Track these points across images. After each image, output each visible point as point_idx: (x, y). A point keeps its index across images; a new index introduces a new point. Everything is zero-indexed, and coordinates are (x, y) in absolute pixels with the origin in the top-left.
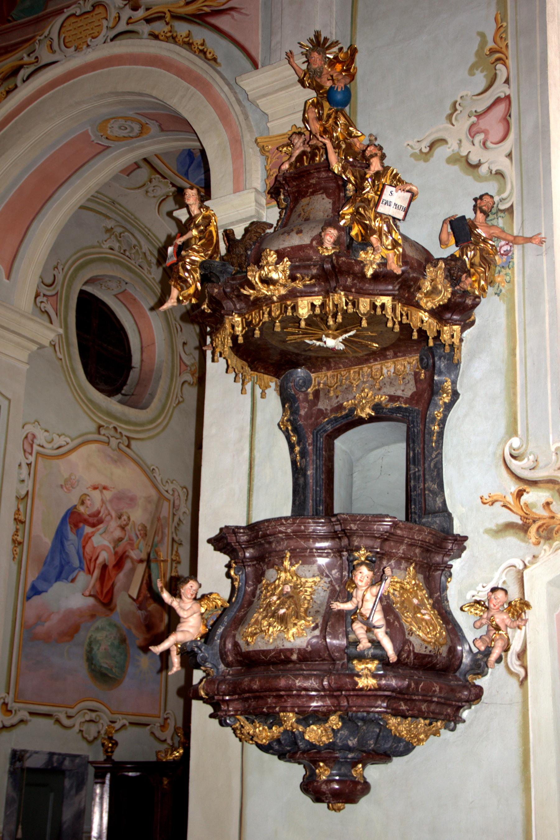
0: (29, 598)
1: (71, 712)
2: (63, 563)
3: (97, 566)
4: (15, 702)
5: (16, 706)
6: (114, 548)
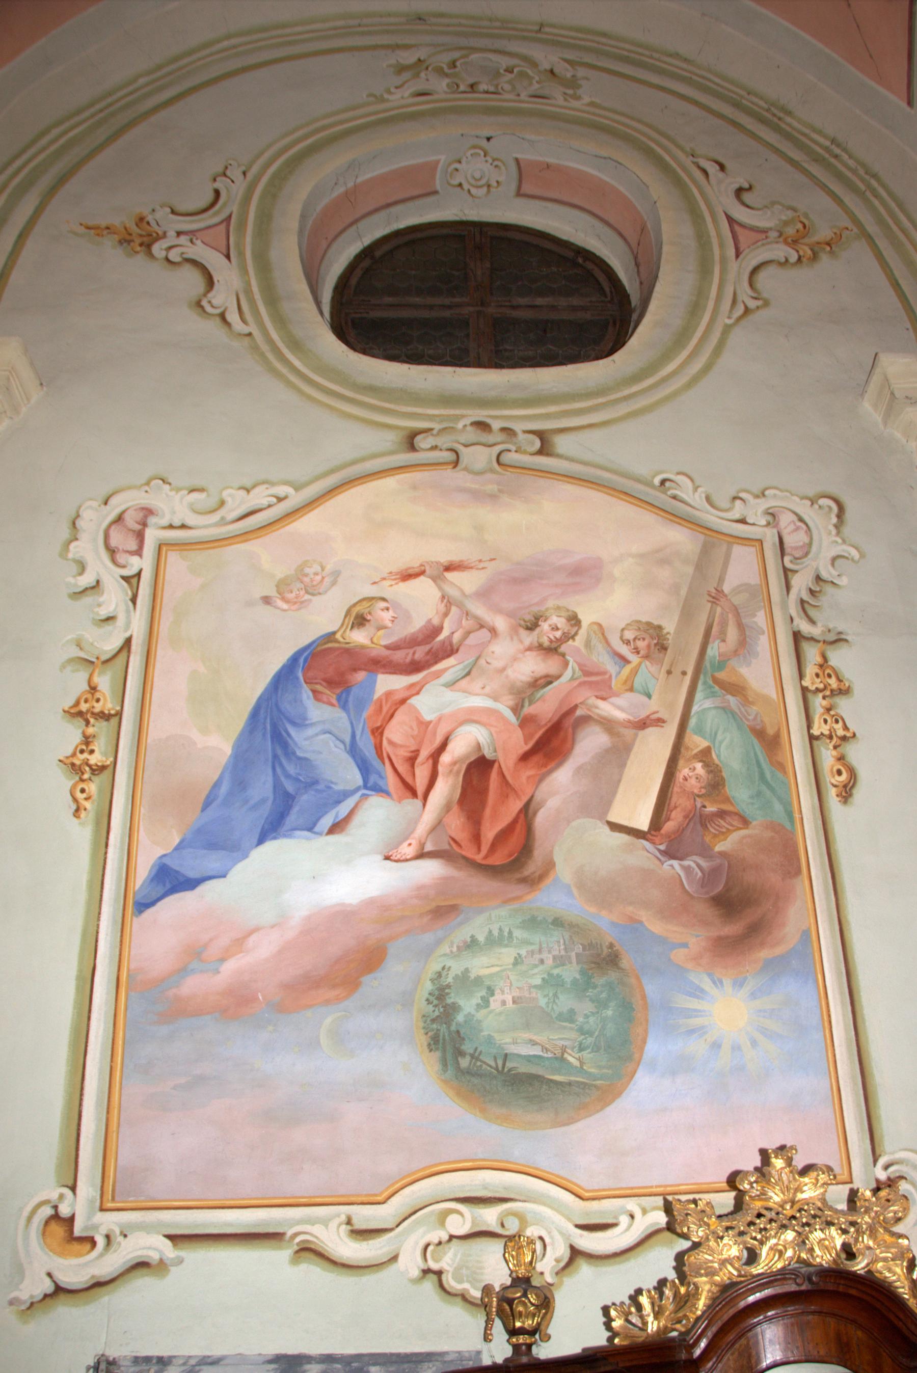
0: (143, 906)
1: (366, 1216)
2: (290, 787)
3: (440, 769)
4: (102, 1209)
5: (110, 1221)
6: (516, 710)
